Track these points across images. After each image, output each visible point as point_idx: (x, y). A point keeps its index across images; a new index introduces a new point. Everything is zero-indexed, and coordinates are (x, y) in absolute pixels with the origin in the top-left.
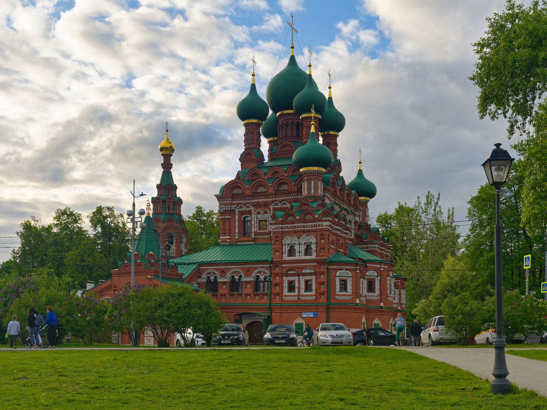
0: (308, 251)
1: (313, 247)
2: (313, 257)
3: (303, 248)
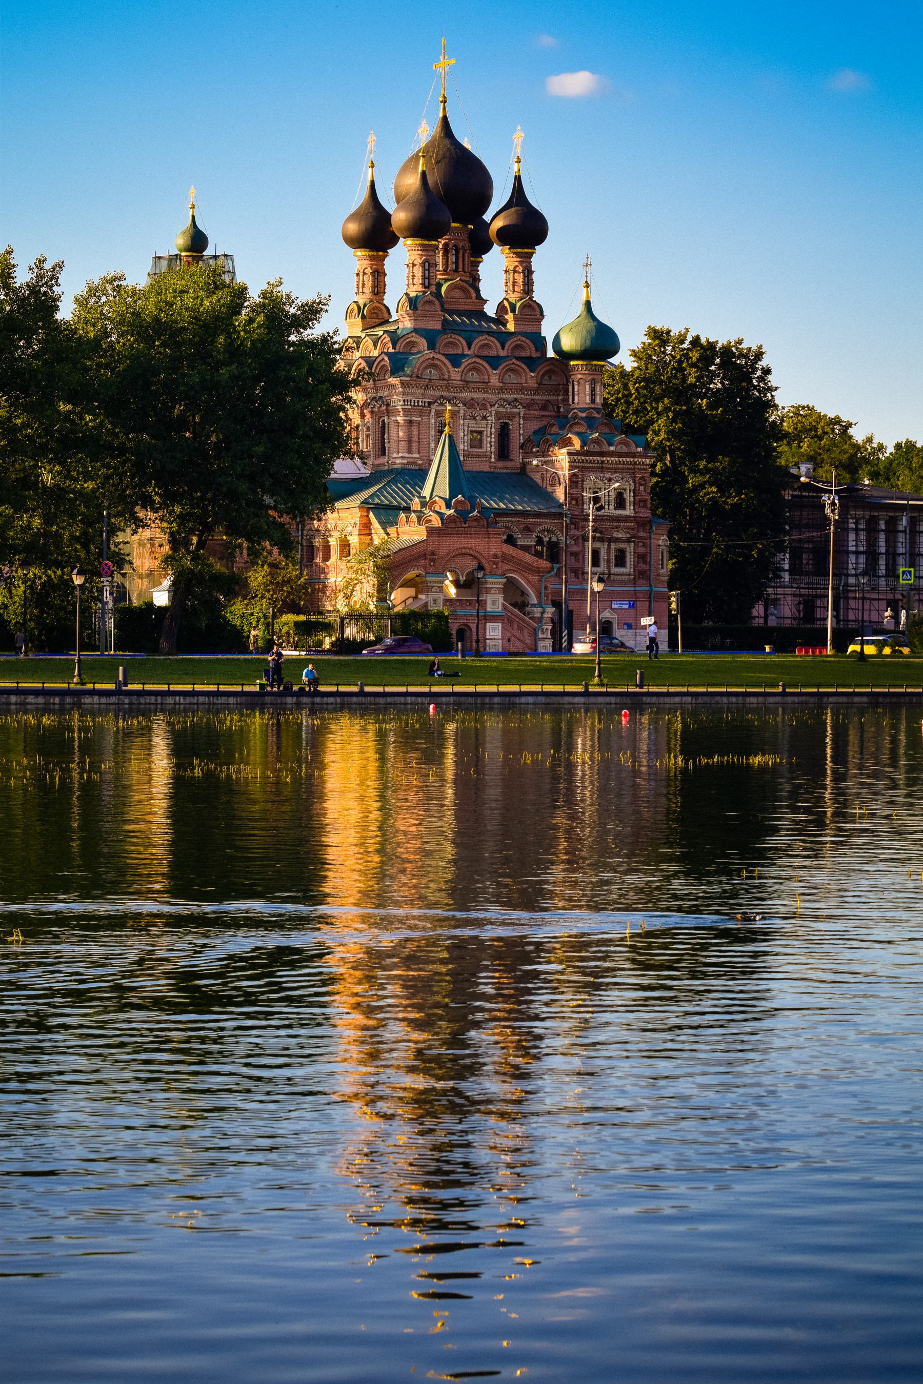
1: (629, 497)
2: (629, 511)
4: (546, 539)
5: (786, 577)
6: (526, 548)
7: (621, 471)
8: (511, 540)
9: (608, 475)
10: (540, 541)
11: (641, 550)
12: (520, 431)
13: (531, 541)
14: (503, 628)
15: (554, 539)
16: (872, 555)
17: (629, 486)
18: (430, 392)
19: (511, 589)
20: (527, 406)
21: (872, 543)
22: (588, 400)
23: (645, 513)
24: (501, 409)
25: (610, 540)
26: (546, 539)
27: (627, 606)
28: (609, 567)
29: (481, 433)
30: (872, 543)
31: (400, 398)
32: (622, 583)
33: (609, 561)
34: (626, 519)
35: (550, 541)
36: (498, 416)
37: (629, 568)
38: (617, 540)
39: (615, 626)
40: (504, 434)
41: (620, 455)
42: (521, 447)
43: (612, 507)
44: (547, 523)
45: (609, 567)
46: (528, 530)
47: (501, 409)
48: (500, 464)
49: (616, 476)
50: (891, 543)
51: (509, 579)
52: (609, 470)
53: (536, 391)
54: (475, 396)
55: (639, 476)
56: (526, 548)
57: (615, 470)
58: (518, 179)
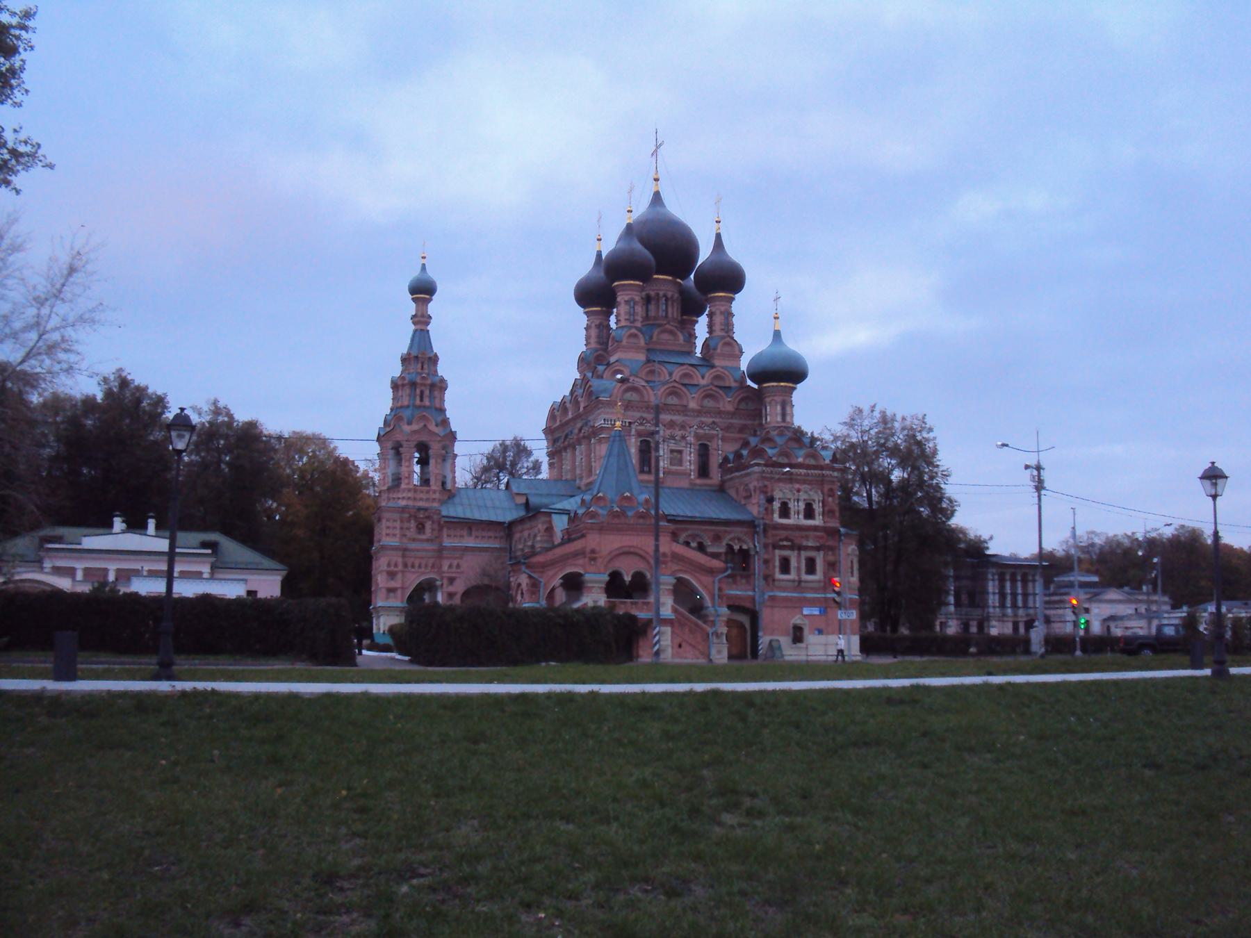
0: (809, 513)
1: (818, 508)
2: (818, 521)
3: (802, 506)
4: (736, 547)
5: (952, 608)
6: (715, 556)
7: (810, 483)
8: (701, 548)
9: (797, 486)
10: (730, 547)
11: (831, 558)
12: (721, 450)
13: (722, 549)
14: (673, 632)
15: (745, 547)
16: (1002, 595)
17: (817, 497)
18: (630, 413)
19: (682, 591)
20: (727, 428)
21: (1002, 587)
22: (779, 419)
23: (834, 523)
24: (701, 431)
25: (801, 548)
26: (736, 547)
27: (817, 613)
28: (799, 575)
29: (680, 452)
30: (1002, 587)
31: (749, 507)
32: (815, 590)
33: (799, 569)
34: (815, 528)
35: (741, 549)
36: (697, 436)
37: (819, 576)
38: (807, 548)
39: (806, 632)
40: (704, 453)
41: (808, 467)
42: (721, 466)
43: (801, 516)
44: (738, 531)
45: (799, 575)
46: (717, 538)
47: (701, 431)
48: (698, 481)
49: (806, 487)
50: (1014, 587)
51: (680, 580)
52: (798, 481)
53: (733, 415)
54: (675, 418)
55: (826, 488)
56: (715, 556)
57: (804, 482)
58: (718, 236)
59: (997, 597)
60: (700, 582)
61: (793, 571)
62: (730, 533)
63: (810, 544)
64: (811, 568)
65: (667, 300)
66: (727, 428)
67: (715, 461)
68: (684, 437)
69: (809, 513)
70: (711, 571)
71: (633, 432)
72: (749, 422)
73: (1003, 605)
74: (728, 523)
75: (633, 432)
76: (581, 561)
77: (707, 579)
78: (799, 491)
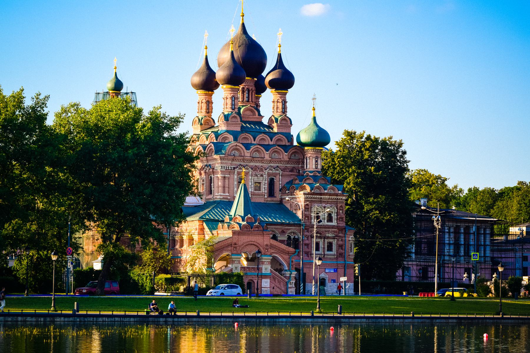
0: (330, 219)
1: (334, 216)
2: (334, 223)
4: (292, 237)
6: (282, 242)
7: (331, 203)
8: (274, 238)
9: (324, 205)
10: (289, 237)
11: (341, 243)
13: (285, 238)
15: (296, 237)
16: (457, 245)
17: (334, 210)
18: (234, 163)
19: (275, 261)
20: (284, 170)
21: (457, 239)
23: (342, 224)
25: (325, 238)
26: (292, 237)
28: (324, 252)
29: (260, 183)
30: (457, 239)
33: (324, 248)
34: (333, 227)
36: (269, 175)
37: (334, 252)
38: (328, 238)
43: (326, 221)
44: (293, 229)
45: (324, 252)
46: (283, 232)
47: (270, 171)
48: (269, 199)
49: (328, 205)
50: (467, 239)
53: (288, 162)
54: (257, 164)
55: (339, 205)
56: (282, 242)
57: (327, 203)
59: (452, 247)
60: (283, 258)
61: (321, 249)
62: (289, 229)
63: (330, 235)
64: (330, 248)
65: (249, 91)
66: (284, 170)
67: (278, 185)
68: (262, 175)
69: (330, 219)
70: (288, 253)
71: (236, 172)
72: (297, 166)
73: (456, 254)
74: (289, 225)
75: (236, 172)
76: (230, 248)
77: (286, 257)
78: (325, 207)
